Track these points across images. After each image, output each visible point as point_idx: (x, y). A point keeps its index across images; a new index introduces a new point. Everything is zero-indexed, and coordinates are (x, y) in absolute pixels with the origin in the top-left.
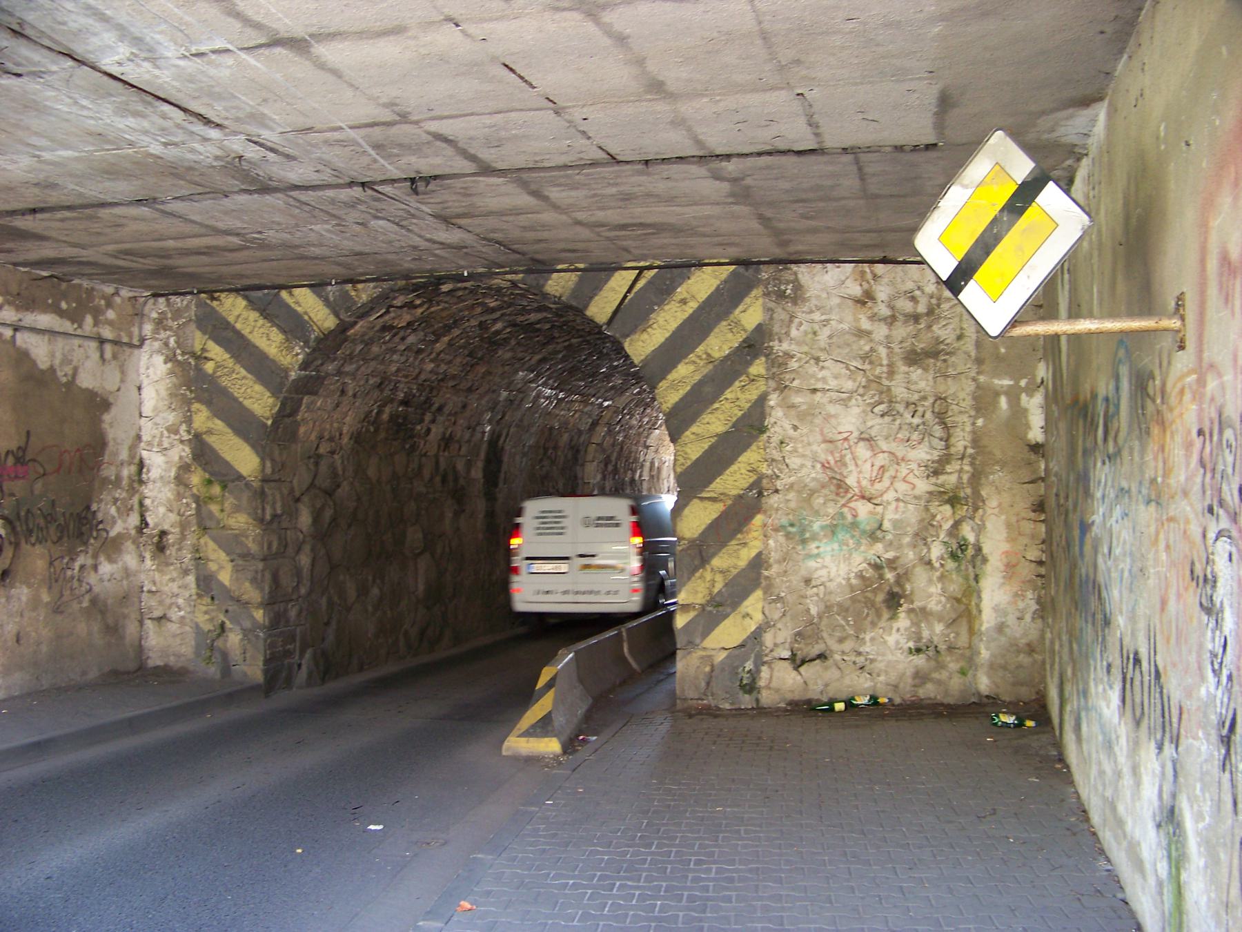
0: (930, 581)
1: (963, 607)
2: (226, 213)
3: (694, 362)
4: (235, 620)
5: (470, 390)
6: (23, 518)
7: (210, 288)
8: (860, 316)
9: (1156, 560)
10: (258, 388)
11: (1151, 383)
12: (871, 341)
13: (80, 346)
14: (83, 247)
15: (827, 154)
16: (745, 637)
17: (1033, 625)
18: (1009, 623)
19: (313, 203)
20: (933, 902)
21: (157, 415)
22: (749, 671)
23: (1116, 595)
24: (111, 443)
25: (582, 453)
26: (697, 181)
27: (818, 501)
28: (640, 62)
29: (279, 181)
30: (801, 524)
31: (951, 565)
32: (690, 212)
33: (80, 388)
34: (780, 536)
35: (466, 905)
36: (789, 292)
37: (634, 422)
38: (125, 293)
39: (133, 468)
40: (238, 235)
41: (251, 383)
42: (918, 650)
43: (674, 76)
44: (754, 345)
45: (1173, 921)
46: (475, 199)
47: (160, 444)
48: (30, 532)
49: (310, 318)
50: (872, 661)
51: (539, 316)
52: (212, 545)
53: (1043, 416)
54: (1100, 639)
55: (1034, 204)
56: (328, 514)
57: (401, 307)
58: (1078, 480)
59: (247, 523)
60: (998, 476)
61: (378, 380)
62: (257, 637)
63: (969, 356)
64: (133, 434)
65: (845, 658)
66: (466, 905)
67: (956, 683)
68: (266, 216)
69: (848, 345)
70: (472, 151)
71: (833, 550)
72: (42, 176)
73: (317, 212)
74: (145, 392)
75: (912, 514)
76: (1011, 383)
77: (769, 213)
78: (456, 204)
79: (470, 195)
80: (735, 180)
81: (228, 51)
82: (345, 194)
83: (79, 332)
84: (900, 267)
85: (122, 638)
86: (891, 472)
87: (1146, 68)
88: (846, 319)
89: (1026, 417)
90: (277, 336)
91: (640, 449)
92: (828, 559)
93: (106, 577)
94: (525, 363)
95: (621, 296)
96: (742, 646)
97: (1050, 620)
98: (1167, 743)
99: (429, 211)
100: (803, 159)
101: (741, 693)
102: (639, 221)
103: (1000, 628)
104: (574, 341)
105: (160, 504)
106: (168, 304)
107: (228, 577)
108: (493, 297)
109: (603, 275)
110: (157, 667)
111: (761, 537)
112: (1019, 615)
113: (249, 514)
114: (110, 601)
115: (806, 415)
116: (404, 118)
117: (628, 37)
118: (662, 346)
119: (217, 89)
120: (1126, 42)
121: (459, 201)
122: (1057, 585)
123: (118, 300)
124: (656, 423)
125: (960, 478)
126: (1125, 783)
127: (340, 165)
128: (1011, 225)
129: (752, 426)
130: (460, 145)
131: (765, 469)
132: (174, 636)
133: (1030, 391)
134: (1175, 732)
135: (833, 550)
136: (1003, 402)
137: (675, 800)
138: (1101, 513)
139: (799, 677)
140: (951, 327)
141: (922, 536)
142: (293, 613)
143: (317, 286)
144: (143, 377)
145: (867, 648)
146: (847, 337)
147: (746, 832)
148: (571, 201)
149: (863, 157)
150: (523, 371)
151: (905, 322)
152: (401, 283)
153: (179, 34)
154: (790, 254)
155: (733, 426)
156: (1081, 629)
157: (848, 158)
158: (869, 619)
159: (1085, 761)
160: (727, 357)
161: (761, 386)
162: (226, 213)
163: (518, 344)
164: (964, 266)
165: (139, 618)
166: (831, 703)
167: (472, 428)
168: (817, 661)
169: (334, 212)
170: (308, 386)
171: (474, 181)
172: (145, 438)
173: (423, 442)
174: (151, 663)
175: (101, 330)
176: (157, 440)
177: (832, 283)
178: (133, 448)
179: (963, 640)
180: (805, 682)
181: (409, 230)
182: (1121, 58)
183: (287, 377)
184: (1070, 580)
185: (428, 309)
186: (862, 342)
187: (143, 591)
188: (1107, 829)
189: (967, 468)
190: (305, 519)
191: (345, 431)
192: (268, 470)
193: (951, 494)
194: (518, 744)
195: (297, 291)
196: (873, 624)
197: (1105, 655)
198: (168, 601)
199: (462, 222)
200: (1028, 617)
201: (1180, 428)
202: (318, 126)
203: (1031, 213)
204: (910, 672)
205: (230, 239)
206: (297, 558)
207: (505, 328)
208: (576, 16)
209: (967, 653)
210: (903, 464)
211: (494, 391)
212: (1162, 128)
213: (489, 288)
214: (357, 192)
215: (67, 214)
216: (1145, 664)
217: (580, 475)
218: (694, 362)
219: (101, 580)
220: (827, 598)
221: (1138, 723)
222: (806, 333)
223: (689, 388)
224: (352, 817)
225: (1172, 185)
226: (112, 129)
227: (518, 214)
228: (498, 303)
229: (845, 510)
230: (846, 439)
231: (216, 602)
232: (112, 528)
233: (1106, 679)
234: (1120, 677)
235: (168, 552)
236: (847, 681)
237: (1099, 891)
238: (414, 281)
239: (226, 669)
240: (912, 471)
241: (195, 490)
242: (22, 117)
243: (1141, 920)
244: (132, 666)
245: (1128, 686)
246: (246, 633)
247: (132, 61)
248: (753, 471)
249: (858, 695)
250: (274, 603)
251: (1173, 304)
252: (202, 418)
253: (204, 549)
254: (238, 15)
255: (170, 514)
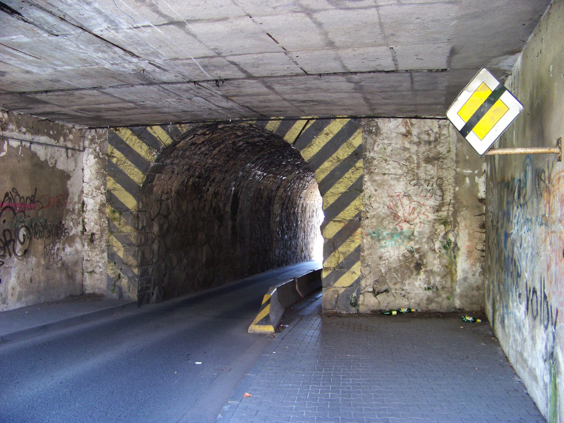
0: (434, 258)
1: (448, 270)
2: (131, 93)
3: (331, 161)
4: (125, 273)
5: (226, 172)
6: (33, 227)
7: (115, 125)
8: (405, 142)
9: (545, 250)
10: (136, 170)
11: (543, 175)
12: (410, 152)
13: (58, 151)
14: (63, 107)
15: (399, 72)
16: (352, 282)
17: (479, 278)
18: (469, 277)
19: (170, 90)
20: (446, 394)
21: (91, 182)
22: (355, 297)
23: (524, 264)
24: (71, 194)
25: (273, 200)
26: (342, 83)
27: (386, 223)
28: (326, 34)
29: (158, 80)
30: (378, 233)
31: (443, 251)
32: (335, 95)
33: (58, 169)
34: (369, 238)
35: (247, 394)
36: (374, 130)
37: (295, 186)
38: (77, 127)
39: (80, 205)
40: (133, 102)
41: (133, 168)
42: (429, 289)
43: (339, 40)
44: (358, 154)
45: (552, 400)
46: (242, 89)
47: (92, 194)
48: (37, 233)
49: (160, 139)
50: (408, 293)
51: (259, 139)
52: (115, 239)
53: (485, 186)
54: (515, 283)
55: (499, 100)
56: (166, 226)
57: (200, 135)
58: (504, 216)
59: (131, 230)
60: (464, 212)
61: (188, 167)
62: (135, 281)
63: (453, 160)
64: (80, 190)
65: (397, 292)
66: (247, 394)
67: (445, 303)
68: (148, 95)
69: (400, 154)
70: (245, 69)
71: (392, 244)
72: (54, 77)
73: (171, 94)
74: (85, 171)
75: (427, 229)
76: (471, 172)
77: (369, 97)
78: (233, 91)
79: (239, 87)
80: (356, 83)
81: (149, 26)
82: (185, 86)
83: (58, 144)
84: (422, 121)
85: (75, 280)
86: (418, 210)
87: (543, 41)
88: (398, 143)
89: (477, 187)
90: (145, 147)
91: (298, 198)
92: (390, 248)
93: (68, 253)
94: (250, 160)
95: (299, 131)
96: (351, 286)
97: (488, 276)
98: (550, 326)
99: (221, 94)
100: (388, 74)
101: (351, 307)
102: (311, 99)
103: (465, 279)
104: (273, 150)
105: (92, 221)
106: (96, 132)
107: (122, 254)
108: (240, 130)
109: (291, 122)
110: (90, 294)
111: (361, 238)
112: (473, 273)
113: (132, 226)
114: (69, 264)
115: (380, 185)
116: (219, 55)
117: (323, 23)
118: (317, 153)
119: (141, 42)
120: (533, 29)
121: (234, 90)
122: (492, 260)
123: (74, 130)
124: (305, 187)
125: (448, 213)
126: (528, 344)
127: (186, 73)
128: (489, 108)
129: (357, 189)
130: (241, 66)
131: (362, 208)
132: (98, 280)
133: (479, 175)
134: (554, 321)
135: (392, 244)
136: (467, 180)
137: (329, 352)
138: (516, 229)
139: (376, 300)
140: (444, 147)
141: (431, 239)
142: (150, 270)
143: (163, 125)
144: (84, 164)
145: (406, 287)
146: (399, 151)
147: (362, 365)
148: (283, 90)
149: (414, 74)
150: (249, 163)
151: (425, 144)
152: (201, 124)
153: (131, 19)
154: (375, 114)
155: (349, 189)
156: (505, 280)
157: (408, 74)
158: (407, 274)
159: (507, 336)
160: (346, 159)
161: (361, 172)
162: (131, 93)
163: (249, 151)
164: (468, 125)
165: (82, 272)
166: (391, 311)
167: (227, 189)
168: (385, 293)
169: (179, 94)
170: (158, 169)
171: (243, 82)
172: (85, 192)
173: (205, 195)
174: (87, 292)
175: (67, 144)
176: (91, 192)
177: (393, 127)
178: (80, 196)
179: (449, 284)
180: (379, 302)
181: (210, 102)
182: (530, 35)
183: (149, 165)
184: (499, 258)
185: (211, 136)
186: (406, 153)
187: (83, 260)
188: (518, 364)
189: (451, 209)
190: (156, 229)
191: (173, 190)
192: (141, 207)
193: (444, 220)
194: (255, 328)
195: (154, 127)
196: (409, 277)
197: (518, 290)
198: (95, 264)
199: (234, 98)
200: (477, 275)
201: (558, 194)
202: (181, 58)
203: (498, 104)
204: (425, 298)
205: (130, 104)
206: (152, 246)
207: (243, 144)
208: (303, 15)
209: (451, 290)
210: (423, 207)
211: (236, 172)
212: (551, 67)
213: (239, 127)
214: (191, 85)
215: (61, 93)
216: (538, 293)
217: (272, 210)
218: (331, 161)
219: (66, 255)
220: (389, 265)
221: (535, 318)
222: (381, 149)
223: (329, 172)
224: (187, 359)
225: (556, 92)
226: (91, 58)
227: (259, 96)
228: (242, 133)
229: (398, 227)
230: (398, 196)
231: (117, 265)
232: (71, 231)
233: (518, 300)
234: (526, 299)
235: (95, 243)
236: (397, 302)
237: (516, 390)
238: (207, 123)
239: (121, 295)
240: (427, 210)
241: (107, 215)
242: (53, 53)
243: (535, 400)
244: (79, 293)
245: (530, 302)
246: (129, 278)
247: (107, 30)
248: (357, 209)
249: (402, 308)
250: (142, 266)
251: (555, 142)
252: (111, 183)
253: (111, 241)
254: (158, 12)
255: (96, 226)
